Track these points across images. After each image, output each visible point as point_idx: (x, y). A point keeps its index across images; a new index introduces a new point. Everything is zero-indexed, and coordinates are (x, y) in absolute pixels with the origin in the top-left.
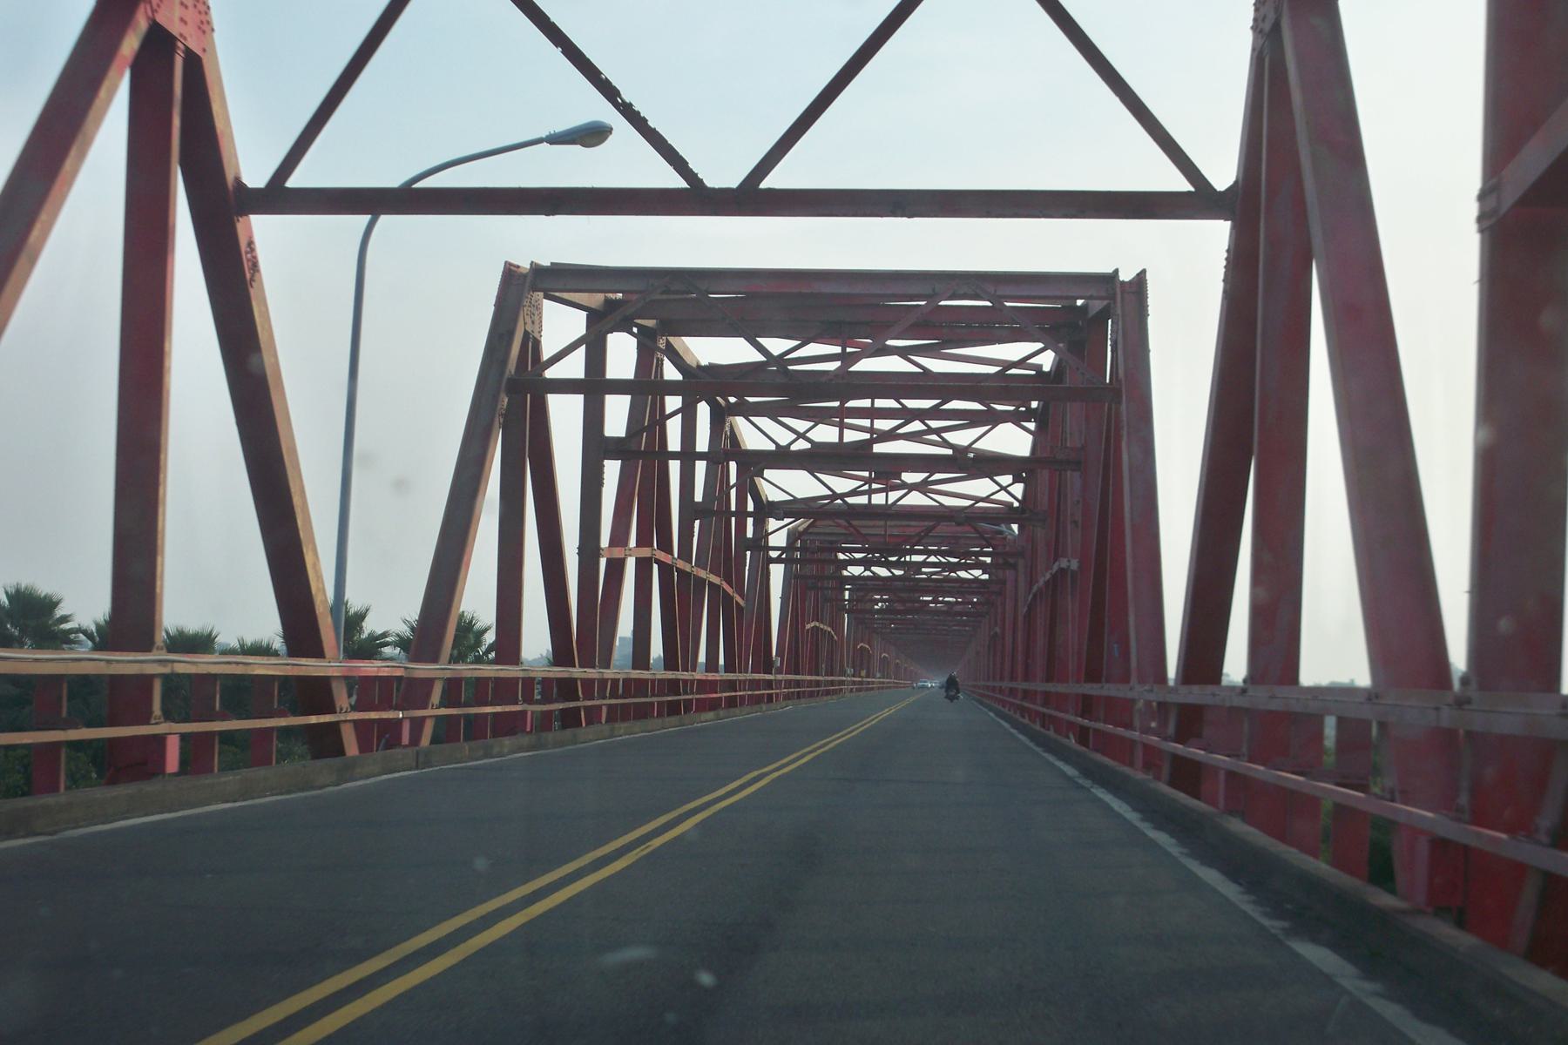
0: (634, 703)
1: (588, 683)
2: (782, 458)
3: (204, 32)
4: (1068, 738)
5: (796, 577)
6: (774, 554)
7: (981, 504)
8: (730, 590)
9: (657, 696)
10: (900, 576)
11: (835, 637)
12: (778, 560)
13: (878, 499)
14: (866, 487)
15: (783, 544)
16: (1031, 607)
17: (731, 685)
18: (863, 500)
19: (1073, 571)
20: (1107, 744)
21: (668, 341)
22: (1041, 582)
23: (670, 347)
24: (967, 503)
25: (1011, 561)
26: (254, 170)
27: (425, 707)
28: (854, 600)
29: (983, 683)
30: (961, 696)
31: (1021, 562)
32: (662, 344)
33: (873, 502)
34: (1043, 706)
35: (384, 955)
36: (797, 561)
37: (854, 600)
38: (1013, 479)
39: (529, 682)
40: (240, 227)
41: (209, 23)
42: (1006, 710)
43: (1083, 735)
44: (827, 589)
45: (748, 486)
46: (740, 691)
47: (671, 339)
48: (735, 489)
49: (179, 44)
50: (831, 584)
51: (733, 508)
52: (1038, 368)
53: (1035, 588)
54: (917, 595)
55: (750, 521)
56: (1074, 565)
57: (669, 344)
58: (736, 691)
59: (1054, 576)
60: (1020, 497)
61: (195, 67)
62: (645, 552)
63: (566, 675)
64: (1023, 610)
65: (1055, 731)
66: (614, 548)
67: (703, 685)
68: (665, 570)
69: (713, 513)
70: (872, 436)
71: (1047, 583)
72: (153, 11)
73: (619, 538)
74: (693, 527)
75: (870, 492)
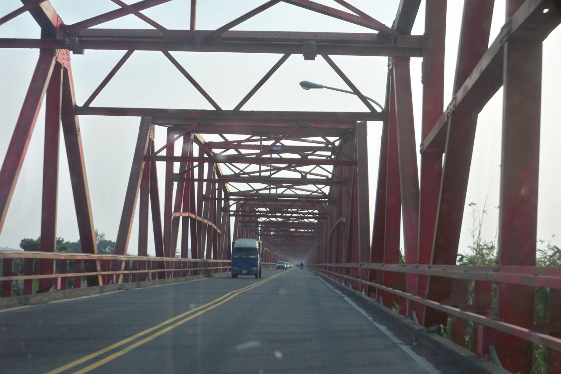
0: (182, 271)
1: (168, 263)
2: (236, 178)
3: (68, 61)
4: (349, 286)
5: (240, 222)
6: (232, 213)
7: (314, 194)
8: (215, 227)
9: (152, 269)
10: (281, 221)
11: (219, 231)
12: (233, 215)
13: (273, 191)
14: (269, 187)
15: (235, 210)
16: (331, 234)
17: (216, 264)
18: (267, 192)
19: (344, 222)
20: (389, 300)
21: (194, 135)
22: (335, 225)
23: (195, 138)
24: (309, 193)
25: (326, 216)
26: (79, 100)
27: (120, 270)
28: (262, 231)
29: (315, 264)
30: (304, 268)
31: (329, 217)
32: (192, 137)
33: (271, 192)
34: (346, 275)
35: (124, 350)
36: (240, 215)
37: (262, 231)
38: (331, 154)
39: (149, 262)
40: (76, 118)
41: (69, 57)
42: (330, 278)
43: (347, 281)
44: (252, 226)
45: (222, 188)
46: (219, 266)
47: (195, 134)
48: (217, 190)
49: (62, 66)
50: (253, 224)
51: (217, 197)
52: (323, 192)
53: (333, 227)
54: (288, 229)
55: (223, 202)
56: (344, 220)
57: (195, 137)
58: (217, 267)
59: (339, 223)
60: (331, 172)
61: (66, 71)
62: (186, 214)
63: (161, 260)
64: (329, 235)
65: (353, 288)
66: (176, 213)
67: (179, 264)
68: (193, 220)
69: (209, 199)
70: (271, 168)
71: (336, 226)
72: (57, 58)
73: (177, 209)
74: (221, 214)
75: (270, 189)
